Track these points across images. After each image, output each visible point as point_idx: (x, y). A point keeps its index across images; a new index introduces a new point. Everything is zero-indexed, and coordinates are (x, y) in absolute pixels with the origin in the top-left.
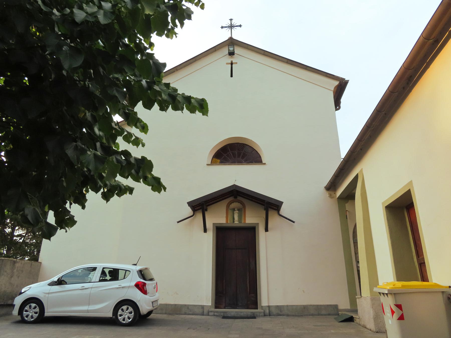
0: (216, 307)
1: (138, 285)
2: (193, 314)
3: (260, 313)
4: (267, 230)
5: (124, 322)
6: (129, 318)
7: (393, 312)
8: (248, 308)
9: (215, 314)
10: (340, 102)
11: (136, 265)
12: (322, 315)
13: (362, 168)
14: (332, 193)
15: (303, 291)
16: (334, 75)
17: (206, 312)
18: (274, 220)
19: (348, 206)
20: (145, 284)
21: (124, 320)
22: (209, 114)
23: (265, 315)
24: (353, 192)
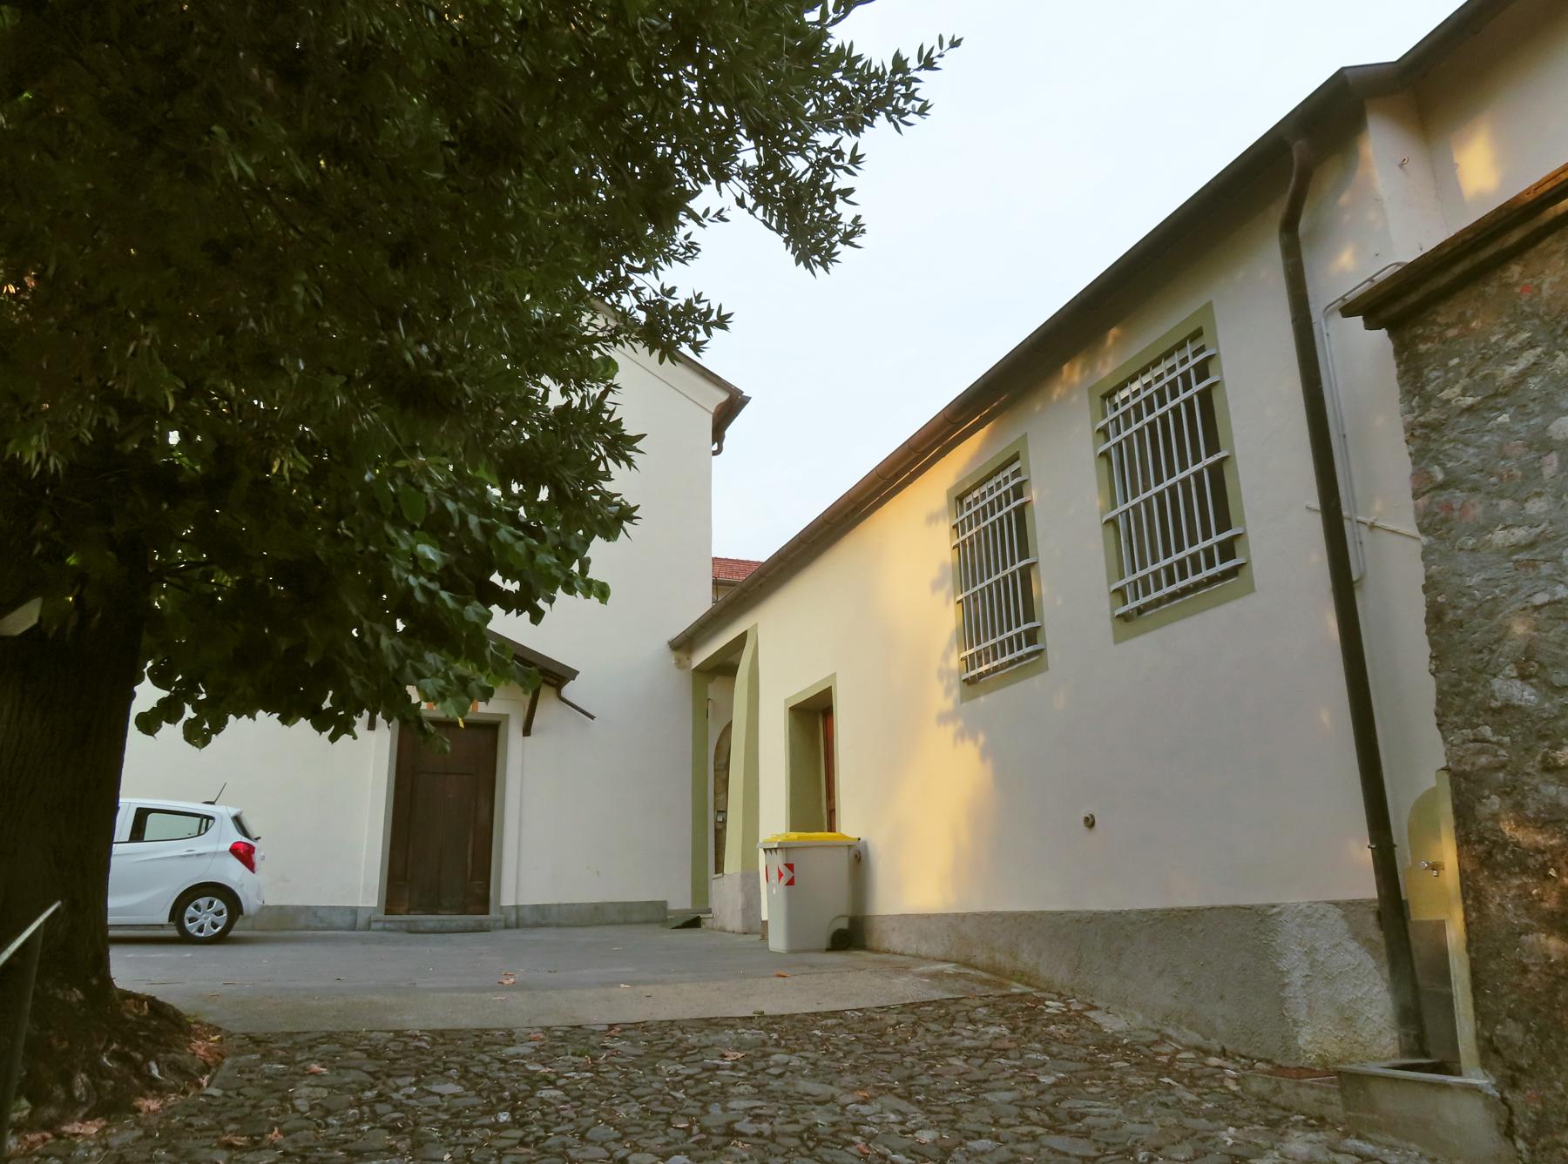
0: (388, 912)
1: (234, 850)
2: (325, 929)
3: (497, 921)
4: (527, 731)
5: (202, 935)
6: (215, 926)
7: (780, 875)
8: (464, 912)
9: (387, 926)
10: (724, 437)
11: (212, 803)
12: (631, 923)
13: (756, 625)
14: (683, 656)
15: (598, 872)
16: (719, 378)
17: (361, 921)
18: (548, 709)
19: (714, 689)
20: (251, 849)
21: (200, 930)
22: (609, 601)
23: (507, 927)
24: (730, 659)
